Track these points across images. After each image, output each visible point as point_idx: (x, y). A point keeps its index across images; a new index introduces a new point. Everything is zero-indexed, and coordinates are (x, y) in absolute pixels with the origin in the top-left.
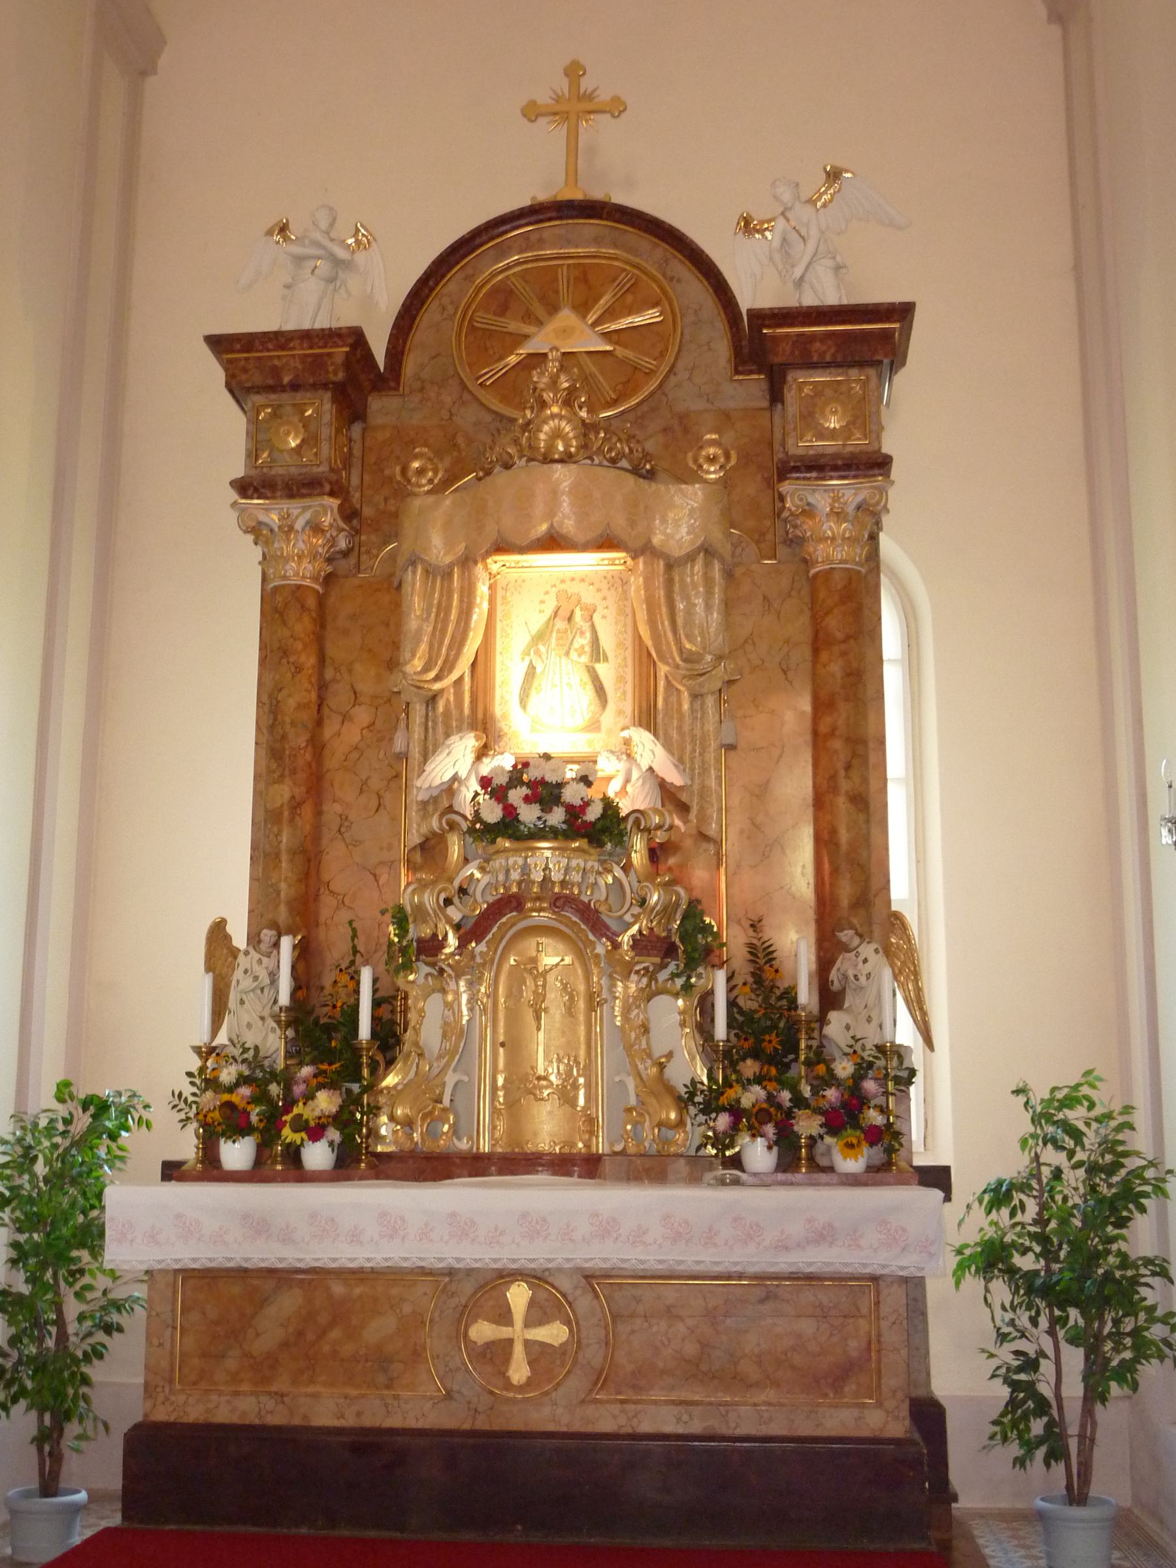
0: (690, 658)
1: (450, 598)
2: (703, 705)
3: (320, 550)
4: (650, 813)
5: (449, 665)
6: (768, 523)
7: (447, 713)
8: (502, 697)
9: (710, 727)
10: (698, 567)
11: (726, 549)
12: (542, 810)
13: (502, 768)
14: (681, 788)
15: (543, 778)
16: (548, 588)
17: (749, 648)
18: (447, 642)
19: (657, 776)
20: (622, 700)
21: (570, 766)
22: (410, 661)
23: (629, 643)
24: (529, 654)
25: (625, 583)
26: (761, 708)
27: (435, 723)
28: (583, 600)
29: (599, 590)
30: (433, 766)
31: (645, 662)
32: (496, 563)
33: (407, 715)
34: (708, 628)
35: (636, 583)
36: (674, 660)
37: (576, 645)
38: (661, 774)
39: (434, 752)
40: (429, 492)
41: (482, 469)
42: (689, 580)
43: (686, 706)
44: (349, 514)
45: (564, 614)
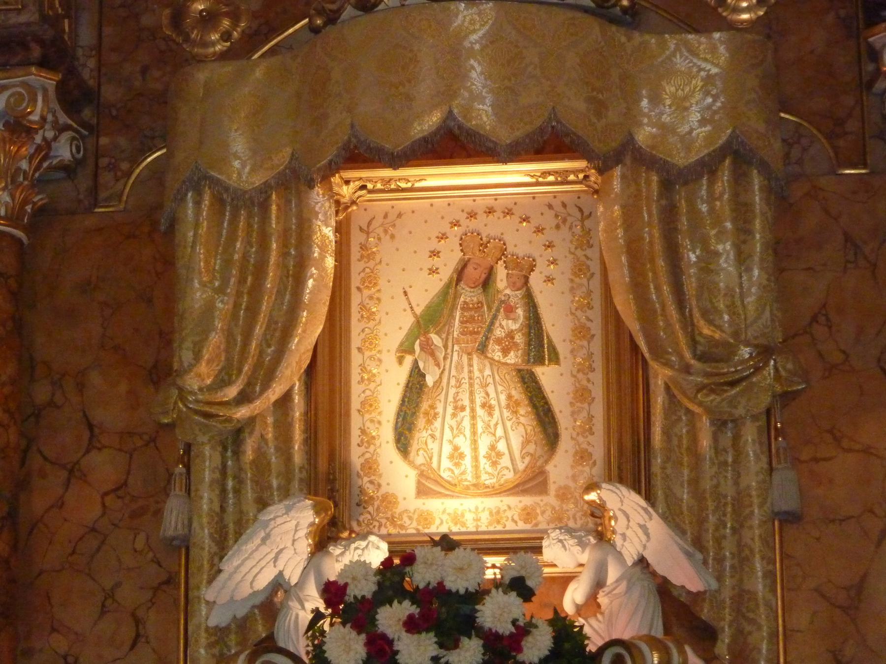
0: (712, 354)
1: (264, 246)
2: (737, 437)
3: (24, 165)
4: (645, 648)
5: (267, 373)
6: (849, 100)
7: (261, 464)
8: (363, 432)
9: (752, 480)
10: (725, 175)
11: (772, 149)
12: (441, 645)
13: (365, 565)
14: (698, 596)
15: (441, 584)
16: (445, 227)
17: (819, 331)
18: (258, 330)
19: (654, 574)
20: (585, 426)
21: (490, 560)
22: (191, 366)
23: (596, 327)
24: (411, 351)
25: (585, 216)
26: (845, 443)
27: (239, 481)
28: (510, 249)
29: (539, 230)
30: (236, 563)
31: (626, 363)
32: (347, 185)
33: (188, 467)
34: (742, 296)
35: (608, 215)
36: (681, 357)
37: (498, 332)
38: (661, 570)
39: (238, 534)
40: (223, 56)
41: (320, 12)
42: (704, 208)
43: (705, 442)
44: (73, 96)
45: (478, 277)
